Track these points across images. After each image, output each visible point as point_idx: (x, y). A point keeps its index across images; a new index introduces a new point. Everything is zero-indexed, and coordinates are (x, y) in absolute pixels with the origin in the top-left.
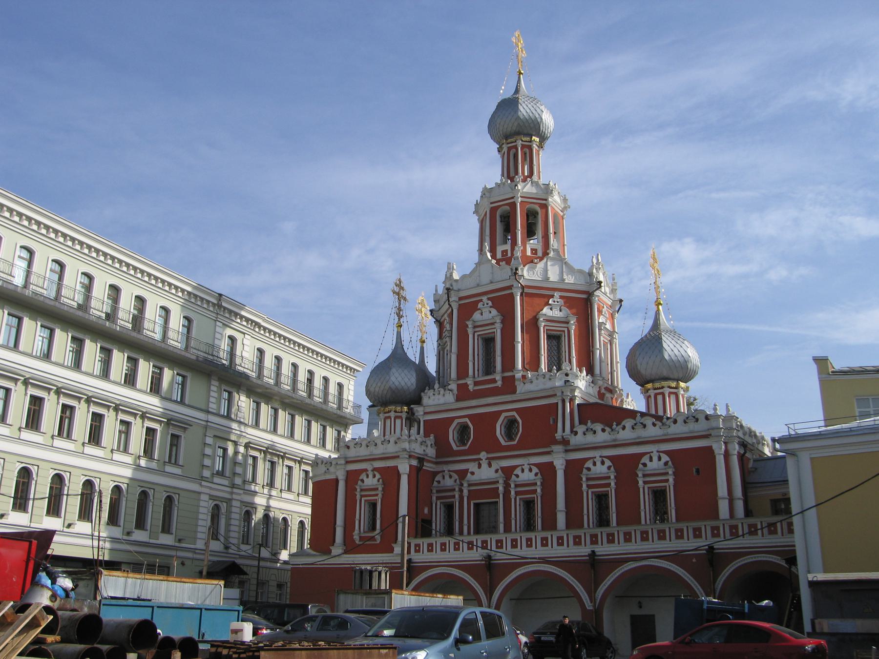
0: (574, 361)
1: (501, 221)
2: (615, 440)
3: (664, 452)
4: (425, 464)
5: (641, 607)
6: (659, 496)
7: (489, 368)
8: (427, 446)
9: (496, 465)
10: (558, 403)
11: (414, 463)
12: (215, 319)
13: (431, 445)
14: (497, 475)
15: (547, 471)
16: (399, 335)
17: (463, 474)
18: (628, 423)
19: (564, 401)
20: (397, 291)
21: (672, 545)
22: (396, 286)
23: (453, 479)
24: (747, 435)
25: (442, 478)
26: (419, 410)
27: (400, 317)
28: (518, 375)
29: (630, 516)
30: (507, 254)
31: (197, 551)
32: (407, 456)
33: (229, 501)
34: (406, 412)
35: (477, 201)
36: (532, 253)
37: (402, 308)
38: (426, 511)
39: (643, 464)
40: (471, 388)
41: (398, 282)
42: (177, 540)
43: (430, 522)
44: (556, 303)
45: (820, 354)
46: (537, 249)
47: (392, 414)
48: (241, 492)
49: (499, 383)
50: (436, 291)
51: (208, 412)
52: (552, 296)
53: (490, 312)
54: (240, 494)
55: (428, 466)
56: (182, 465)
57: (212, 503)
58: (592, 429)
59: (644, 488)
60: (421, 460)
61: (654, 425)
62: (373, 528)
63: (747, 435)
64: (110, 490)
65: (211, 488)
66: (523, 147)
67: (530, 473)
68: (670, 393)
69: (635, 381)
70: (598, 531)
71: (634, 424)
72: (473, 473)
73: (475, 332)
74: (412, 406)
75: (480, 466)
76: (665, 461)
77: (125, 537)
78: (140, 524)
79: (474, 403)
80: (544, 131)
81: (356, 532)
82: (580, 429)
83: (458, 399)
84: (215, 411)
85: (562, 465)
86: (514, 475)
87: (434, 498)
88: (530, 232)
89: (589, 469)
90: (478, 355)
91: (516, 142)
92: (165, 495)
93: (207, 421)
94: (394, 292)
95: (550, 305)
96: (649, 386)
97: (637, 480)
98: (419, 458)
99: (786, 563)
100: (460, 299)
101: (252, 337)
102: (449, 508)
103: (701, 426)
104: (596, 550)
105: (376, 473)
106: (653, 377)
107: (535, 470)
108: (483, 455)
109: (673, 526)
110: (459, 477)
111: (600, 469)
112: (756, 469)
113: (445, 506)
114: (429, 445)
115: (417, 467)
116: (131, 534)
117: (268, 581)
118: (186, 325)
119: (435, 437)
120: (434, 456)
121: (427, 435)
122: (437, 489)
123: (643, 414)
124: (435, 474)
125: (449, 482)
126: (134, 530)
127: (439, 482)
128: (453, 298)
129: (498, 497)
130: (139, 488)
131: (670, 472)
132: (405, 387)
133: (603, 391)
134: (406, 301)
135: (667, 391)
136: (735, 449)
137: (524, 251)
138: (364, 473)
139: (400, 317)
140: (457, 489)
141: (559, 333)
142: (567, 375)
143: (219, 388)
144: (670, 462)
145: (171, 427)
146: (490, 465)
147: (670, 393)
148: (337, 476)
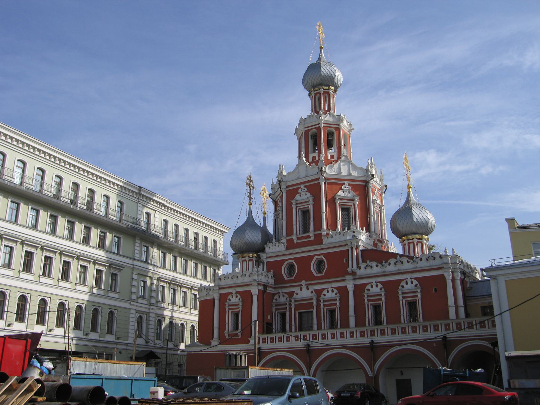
0: (358, 223)
1: (312, 139)
2: (384, 272)
3: (416, 279)
4: (268, 289)
5: (402, 374)
6: (412, 305)
7: (306, 229)
8: (269, 278)
9: (311, 288)
11: (261, 288)
12: (137, 202)
13: (271, 277)
14: (312, 295)
15: (343, 291)
16: (250, 210)
17: (291, 294)
18: (392, 261)
19: (352, 249)
20: (249, 183)
21: (420, 336)
22: (248, 180)
23: (285, 298)
24: (466, 267)
26: (263, 256)
27: (251, 198)
28: (324, 233)
29: (394, 318)
31: (129, 345)
32: (257, 284)
33: (148, 314)
34: (256, 257)
35: (297, 126)
36: (331, 158)
37: (252, 193)
38: (269, 317)
39: (401, 286)
40: (295, 241)
42: (116, 338)
44: (346, 188)
45: (509, 216)
46: (334, 155)
47: (247, 259)
48: (155, 308)
49: (312, 238)
50: (273, 182)
51: (134, 259)
52: (344, 184)
54: (154, 309)
55: (269, 290)
56: (119, 292)
57: (137, 315)
60: (265, 286)
61: (408, 262)
62: (237, 328)
63: (466, 267)
64: (75, 308)
65: (137, 306)
66: (324, 93)
67: (332, 293)
69: (396, 235)
70: (375, 328)
72: (297, 294)
73: (297, 207)
74: (259, 253)
75: (301, 289)
77: (85, 337)
78: (94, 329)
79: (297, 250)
80: (337, 83)
81: (226, 331)
82: (363, 265)
83: (287, 248)
84: (138, 259)
85: (352, 287)
87: (274, 310)
88: (330, 145)
89: (368, 290)
91: (319, 90)
92: (109, 310)
93: (134, 265)
94: (247, 184)
95: (343, 189)
96: (405, 238)
97: (399, 296)
98: (264, 285)
99: (492, 346)
101: (160, 213)
102: (283, 315)
103: (437, 263)
104: (374, 340)
105: (238, 295)
106: (407, 233)
107: (335, 291)
109: (421, 324)
110: (289, 296)
111: (375, 290)
112: (472, 288)
113: (280, 314)
114: (270, 277)
115: (263, 290)
116: (88, 335)
117: (173, 362)
118: (120, 206)
119: (273, 272)
120: (273, 284)
121: (268, 271)
122: (276, 304)
123: (401, 256)
124: (274, 295)
125: (282, 300)
126: (90, 333)
127: (276, 300)
128: (283, 186)
129: (313, 308)
130: (92, 306)
131: (419, 291)
133: (376, 242)
134: (254, 189)
135: (415, 241)
136: (458, 276)
138: (231, 295)
139: (251, 198)
140: (288, 304)
141: (348, 206)
142: (354, 232)
143: (141, 244)
145: (112, 269)
146: (308, 289)
147: (418, 242)
148: (214, 297)
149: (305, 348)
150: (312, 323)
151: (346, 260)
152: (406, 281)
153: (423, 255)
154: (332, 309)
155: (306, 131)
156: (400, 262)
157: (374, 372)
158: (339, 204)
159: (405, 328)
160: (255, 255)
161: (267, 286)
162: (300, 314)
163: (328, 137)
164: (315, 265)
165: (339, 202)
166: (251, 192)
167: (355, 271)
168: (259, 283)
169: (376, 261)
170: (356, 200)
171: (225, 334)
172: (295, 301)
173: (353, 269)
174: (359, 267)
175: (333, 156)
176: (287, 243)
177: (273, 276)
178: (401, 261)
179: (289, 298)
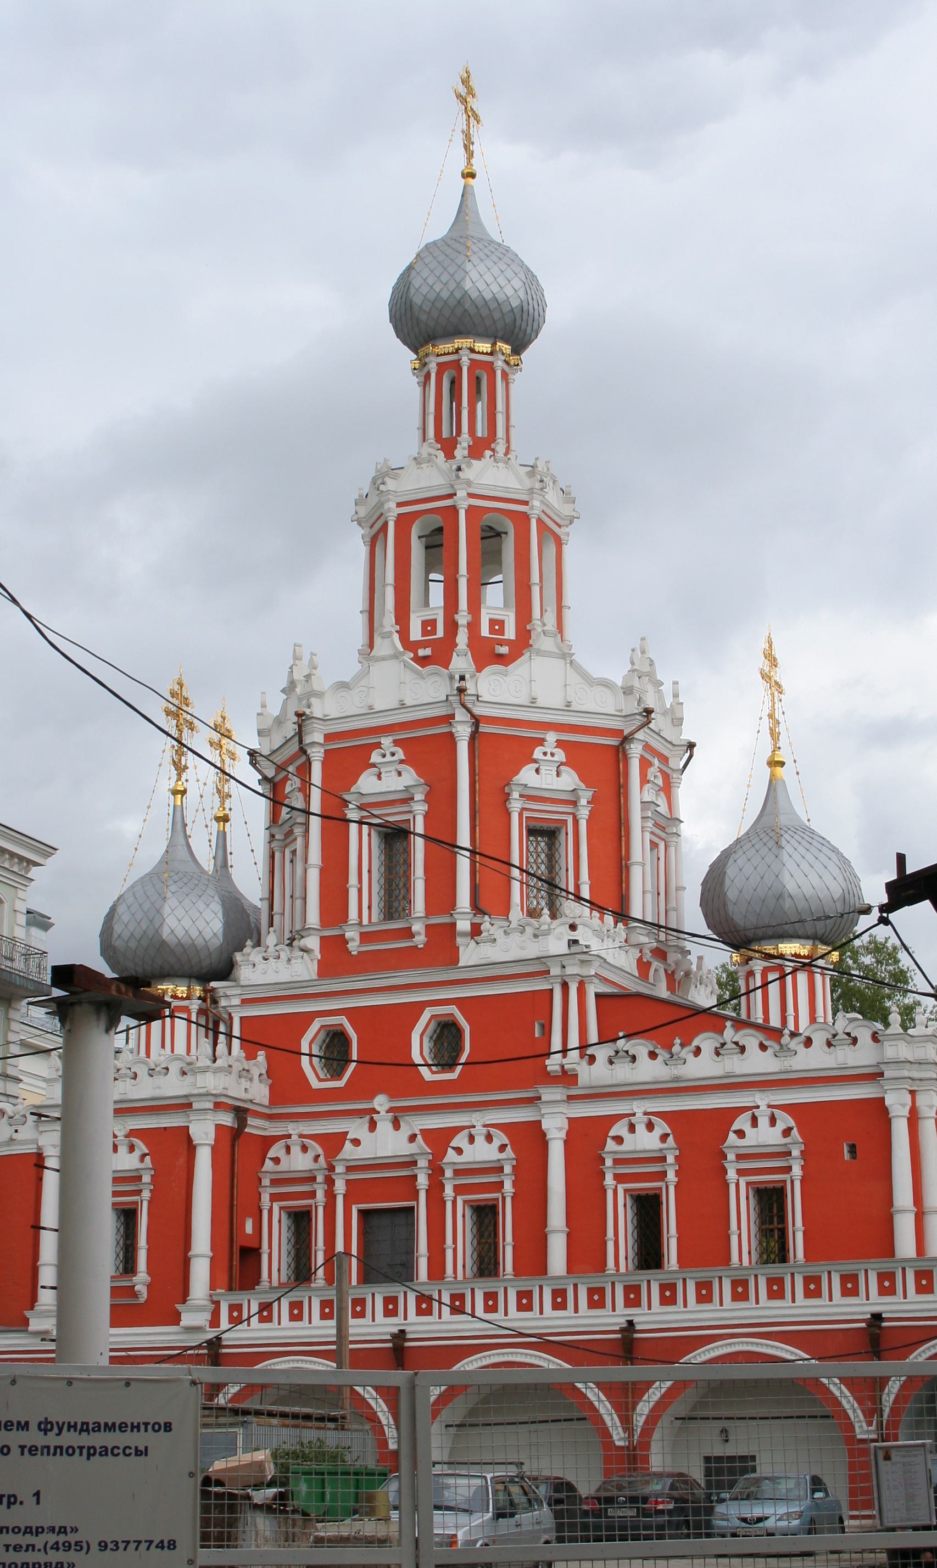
2: (677, 1079)
3: (787, 1108)
4: (251, 1121)
8: (251, 1080)
10: (551, 990)
11: (227, 1119)
13: (260, 1075)
17: (332, 1144)
18: (706, 1042)
19: (565, 986)
23: (310, 1155)
28: (463, 925)
30: (434, 631)
32: (212, 1107)
34: (200, 998)
36: (492, 631)
39: (735, 1132)
40: (354, 946)
41: (177, 687)
44: (549, 757)
49: (420, 940)
52: (541, 742)
53: (400, 774)
55: (255, 1126)
58: (627, 1052)
59: (737, 1185)
60: (241, 1113)
61: (763, 1047)
70: (642, 1277)
72: (356, 1142)
74: (213, 984)
75: (373, 1126)
76: (784, 1127)
80: (523, 326)
86: (454, 1148)
87: (265, 1198)
89: (619, 1140)
90: (370, 871)
104: (636, 1320)
105: (136, 1141)
107: (500, 1138)
108: (381, 1102)
115: (232, 1128)
124: (269, 1142)
125: (299, 1162)
129: (416, 1198)
133: (648, 956)
140: (320, 1178)
142: (573, 927)
146: (396, 1125)
149: (390, 1345)
151: (543, 1026)
152: (753, 1114)
153: (814, 1026)
154: (482, 1204)
156: (734, 1046)
158: (521, 815)
160: (198, 990)
161: (246, 1111)
162: (365, 1215)
164: (426, 1040)
165: (523, 809)
167: (574, 1070)
170: (583, 802)
172: (350, 1169)
174: (590, 1056)
175: (501, 623)
179: (326, 1158)
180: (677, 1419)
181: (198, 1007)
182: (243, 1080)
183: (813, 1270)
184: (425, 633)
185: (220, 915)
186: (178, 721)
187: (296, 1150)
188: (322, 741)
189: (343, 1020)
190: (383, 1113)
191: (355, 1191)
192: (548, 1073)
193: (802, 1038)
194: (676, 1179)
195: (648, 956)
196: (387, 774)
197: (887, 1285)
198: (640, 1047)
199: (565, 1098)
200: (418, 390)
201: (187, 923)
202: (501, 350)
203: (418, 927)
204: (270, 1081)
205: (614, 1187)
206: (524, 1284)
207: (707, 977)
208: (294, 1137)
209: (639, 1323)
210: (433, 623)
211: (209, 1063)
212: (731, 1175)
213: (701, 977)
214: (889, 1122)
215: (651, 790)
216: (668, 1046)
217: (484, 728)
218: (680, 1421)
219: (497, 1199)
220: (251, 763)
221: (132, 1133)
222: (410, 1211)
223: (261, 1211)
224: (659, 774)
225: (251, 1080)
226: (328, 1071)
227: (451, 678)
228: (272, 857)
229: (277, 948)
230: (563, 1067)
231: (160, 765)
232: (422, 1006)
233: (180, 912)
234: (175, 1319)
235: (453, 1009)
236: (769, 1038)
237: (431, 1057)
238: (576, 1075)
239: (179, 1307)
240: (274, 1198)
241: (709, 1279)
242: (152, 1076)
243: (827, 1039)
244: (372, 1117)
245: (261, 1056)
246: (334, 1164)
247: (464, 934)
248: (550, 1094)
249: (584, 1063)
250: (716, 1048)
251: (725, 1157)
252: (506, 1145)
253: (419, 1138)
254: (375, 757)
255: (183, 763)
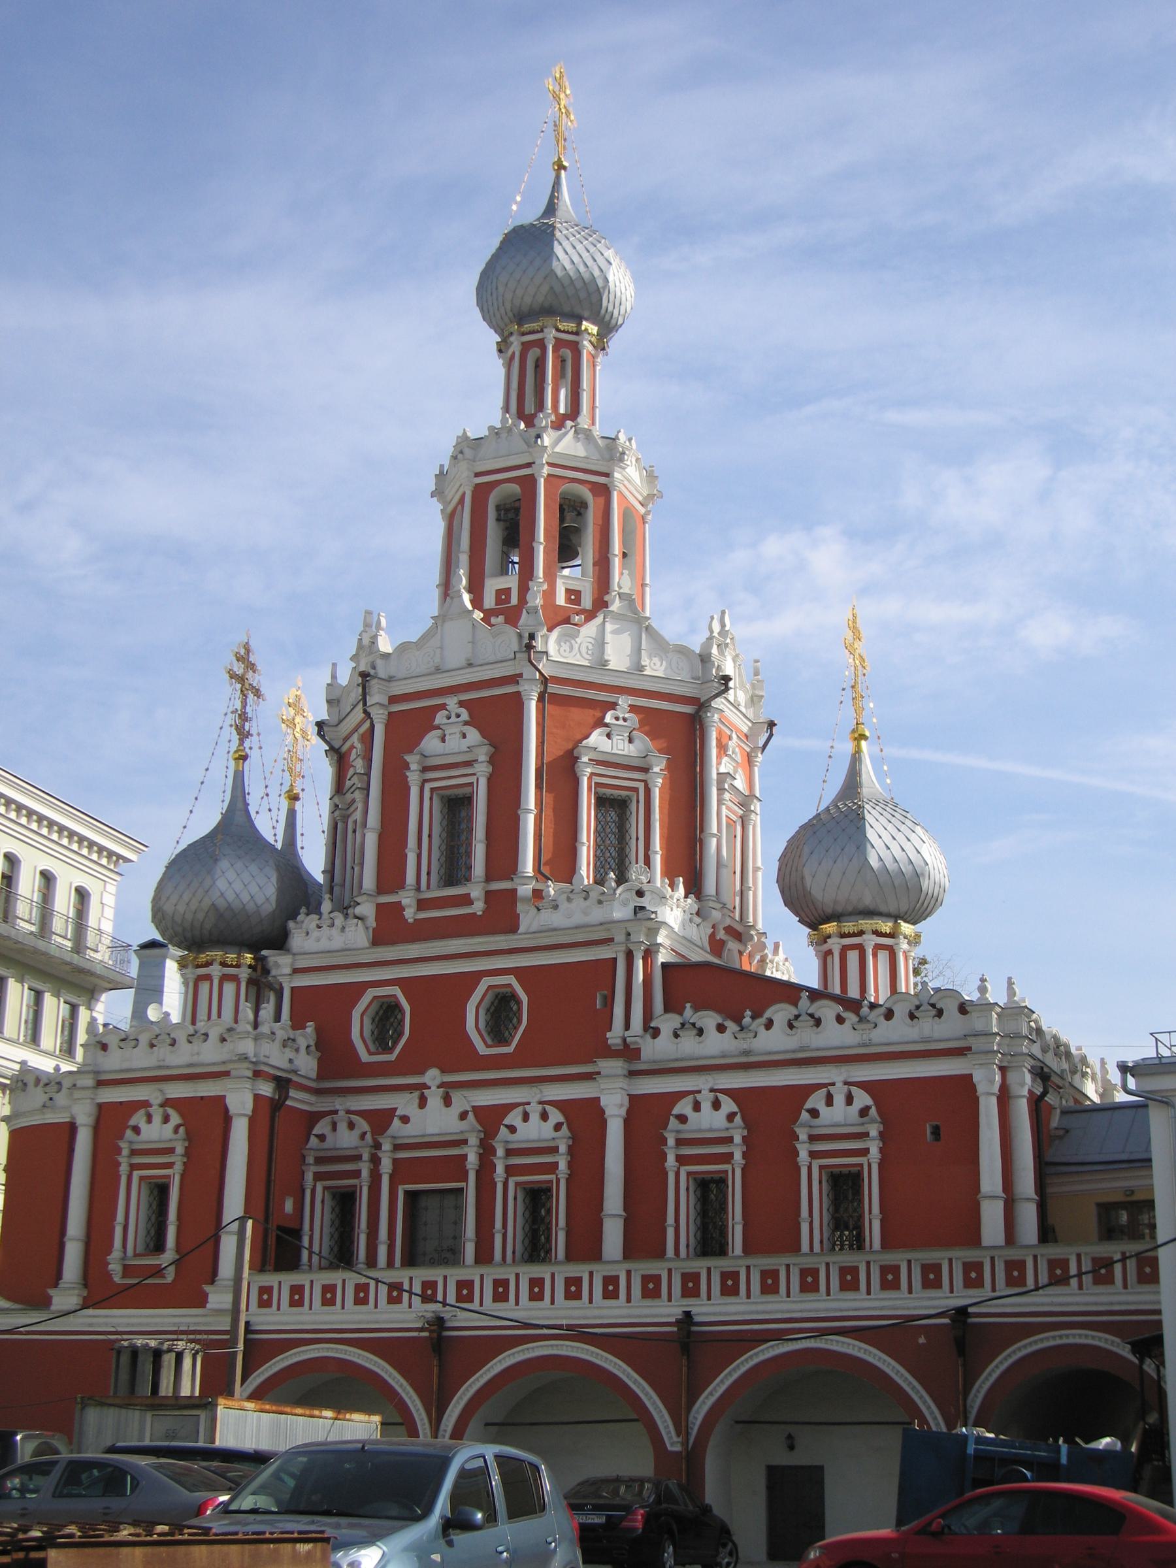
1: (498, 520)
2: (746, 1053)
3: (865, 1086)
4: (292, 1093)
8: (297, 1050)
10: (615, 959)
11: (267, 1089)
13: (308, 1047)
17: (380, 1120)
19: (630, 956)
20: (240, 672)
23: (357, 1133)
25: (329, 1128)
27: (243, 735)
28: (525, 890)
30: (508, 600)
34: (250, 966)
35: (442, 466)
36: (568, 600)
38: (289, 1206)
39: (808, 1111)
40: (410, 914)
41: (242, 652)
43: (297, 1233)
44: (621, 722)
47: (216, 971)
49: (478, 907)
52: (613, 706)
53: (464, 736)
55: (298, 1100)
60: (282, 1084)
61: (840, 1020)
62: (158, 1246)
66: (558, 344)
68: (878, 947)
70: (700, 1265)
71: (913, 1008)
72: (405, 1119)
74: (264, 952)
75: (423, 1101)
80: (610, 309)
82: (667, 1023)
83: (377, 940)
86: (507, 1126)
87: (309, 1177)
88: (566, 550)
89: (683, 1119)
90: (430, 836)
91: (542, 331)
94: (233, 675)
95: (607, 725)
96: (830, 928)
100: (393, 700)
103: (948, 1029)
104: (694, 1310)
105: (170, 1111)
106: (840, 909)
108: (433, 1076)
112: (1067, 1131)
115: (272, 1099)
121: (297, 1023)
124: (315, 1117)
125: (346, 1139)
127: (322, 1138)
129: (465, 1179)
131: (874, 1133)
132: (251, 907)
133: (721, 935)
135: (870, 941)
137: (550, 594)
139: (243, 735)
140: (366, 1157)
142: (640, 893)
144: (565, 1125)
146: (447, 1101)
148: (73, 1117)
150: (458, 1236)
151: (605, 998)
155: (477, 486)
157: (688, 1434)
158: (590, 779)
159: (815, 1272)
160: (248, 957)
161: (289, 1081)
163: (562, 519)
164: (482, 1012)
165: (592, 774)
166: (248, 709)
168: (258, 1068)
169: (718, 1011)
171: (111, 1267)
173: (627, 1034)
175: (578, 593)
176: (377, 919)
177: (316, 1045)
178: (811, 1016)
180: (737, 1422)
181: (247, 976)
182: (287, 1050)
183: (891, 1258)
184: (498, 601)
185: (274, 879)
186: (243, 685)
187: (342, 1126)
188: (386, 703)
189: (396, 991)
190: (434, 1088)
191: (401, 1170)
192: (609, 1047)
193: (882, 1010)
194: (743, 1162)
195: (721, 935)
196: (452, 736)
197: (973, 1276)
198: (709, 1020)
199: (625, 1072)
200: (502, 372)
201: (238, 886)
202: (586, 330)
203: (476, 891)
204: (319, 1054)
205: (675, 1169)
206: (574, 1270)
207: (784, 964)
208: (341, 1113)
209: (698, 1314)
210: (507, 591)
211: (249, 1028)
212: (803, 1156)
213: (778, 964)
214: (976, 1101)
215: (727, 764)
216: (738, 1020)
217: (553, 688)
218: (741, 1425)
219: (552, 1181)
220: (319, 734)
221: (167, 1103)
222: (460, 1191)
223: (303, 1191)
224: (737, 750)
225: (297, 1050)
226: (380, 1045)
227: (520, 636)
228: (335, 828)
229: (332, 915)
230: (624, 1040)
231: (221, 728)
232: (477, 976)
233: (231, 875)
234: (201, 1301)
235: (511, 980)
236: (846, 1009)
237: (487, 1031)
238: (639, 1050)
239: (207, 1288)
240: (318, 1177)
241: (775, 1267)
242: (191, 1042)
243: (910, 1011)
244: (423, 1093)
245: (310, 1028)
246: (381, 1140)
247: (525, 900)
248: (612, 1067)
249: (648, 1037)
250: (790, 1020)
251: (797, 1138)
252: (562, 1124)
253: (471, 1116)
254: (440, 718)
255: (247, 728)
